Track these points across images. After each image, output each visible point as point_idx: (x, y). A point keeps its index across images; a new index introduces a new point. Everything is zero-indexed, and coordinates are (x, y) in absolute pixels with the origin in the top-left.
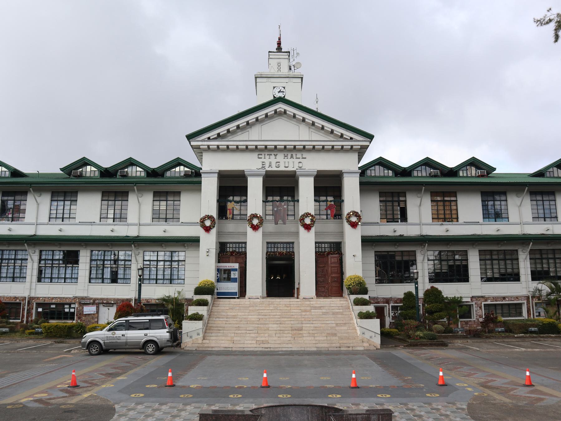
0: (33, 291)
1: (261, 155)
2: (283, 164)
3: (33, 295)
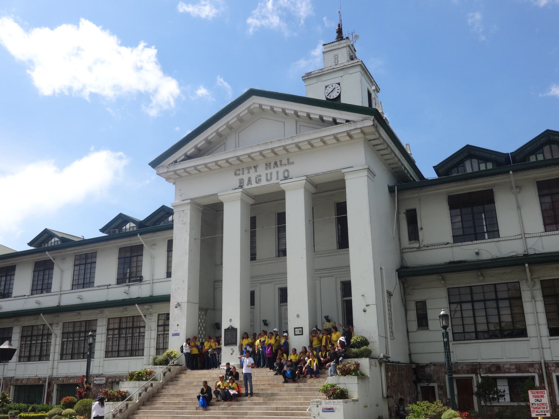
0: (55, 370)
3: (55, 375)
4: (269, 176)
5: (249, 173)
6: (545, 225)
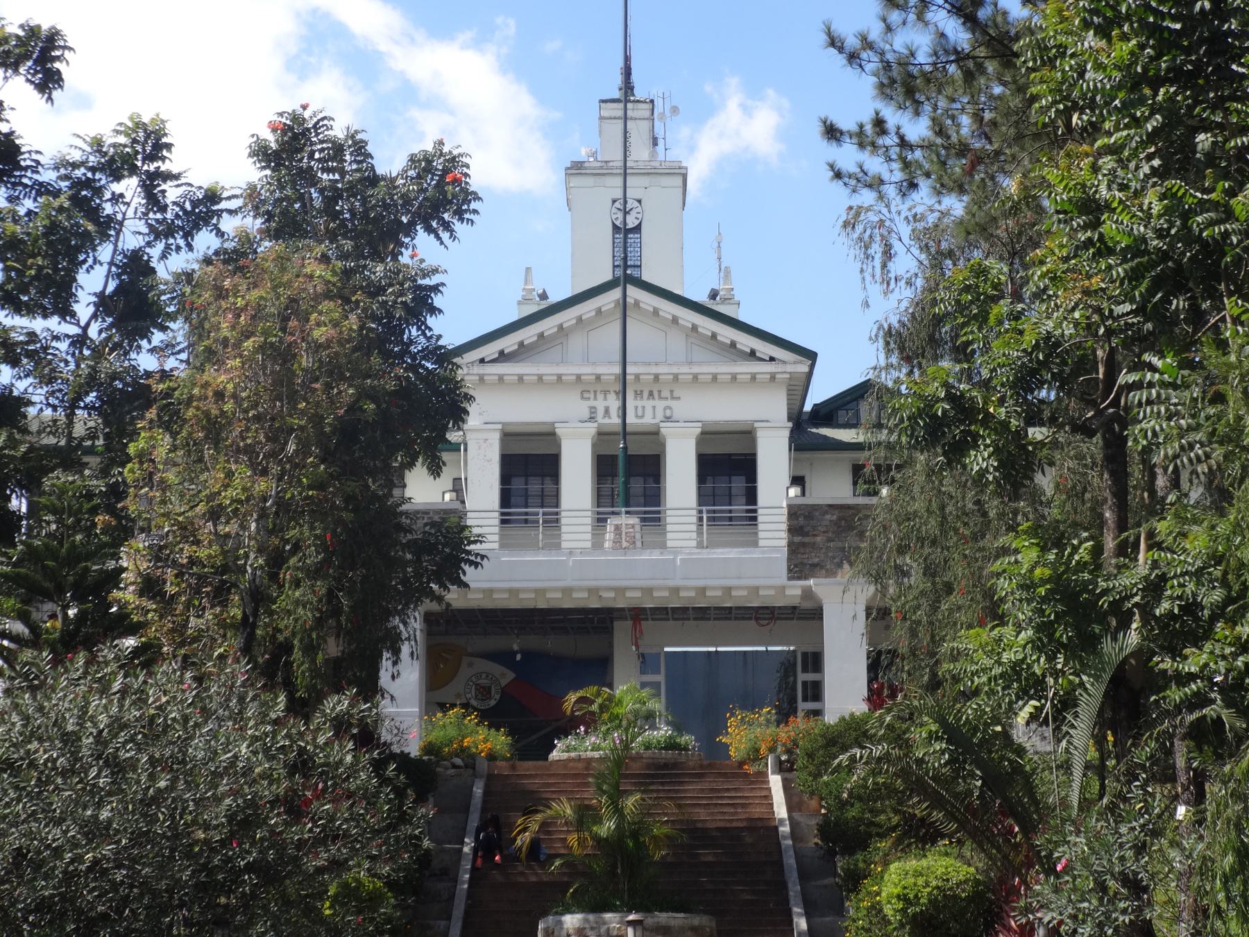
4: (640, 410)
5: (605, 399)
6: (790, 571)
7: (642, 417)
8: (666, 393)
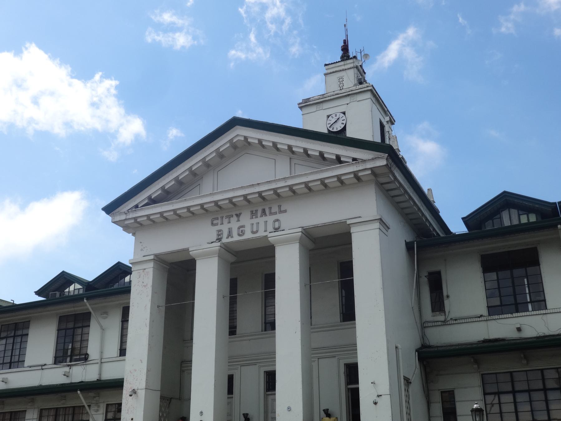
1: (217, 219)
2: (248, 229)
7: (257, 232)
8: (275, 209)
